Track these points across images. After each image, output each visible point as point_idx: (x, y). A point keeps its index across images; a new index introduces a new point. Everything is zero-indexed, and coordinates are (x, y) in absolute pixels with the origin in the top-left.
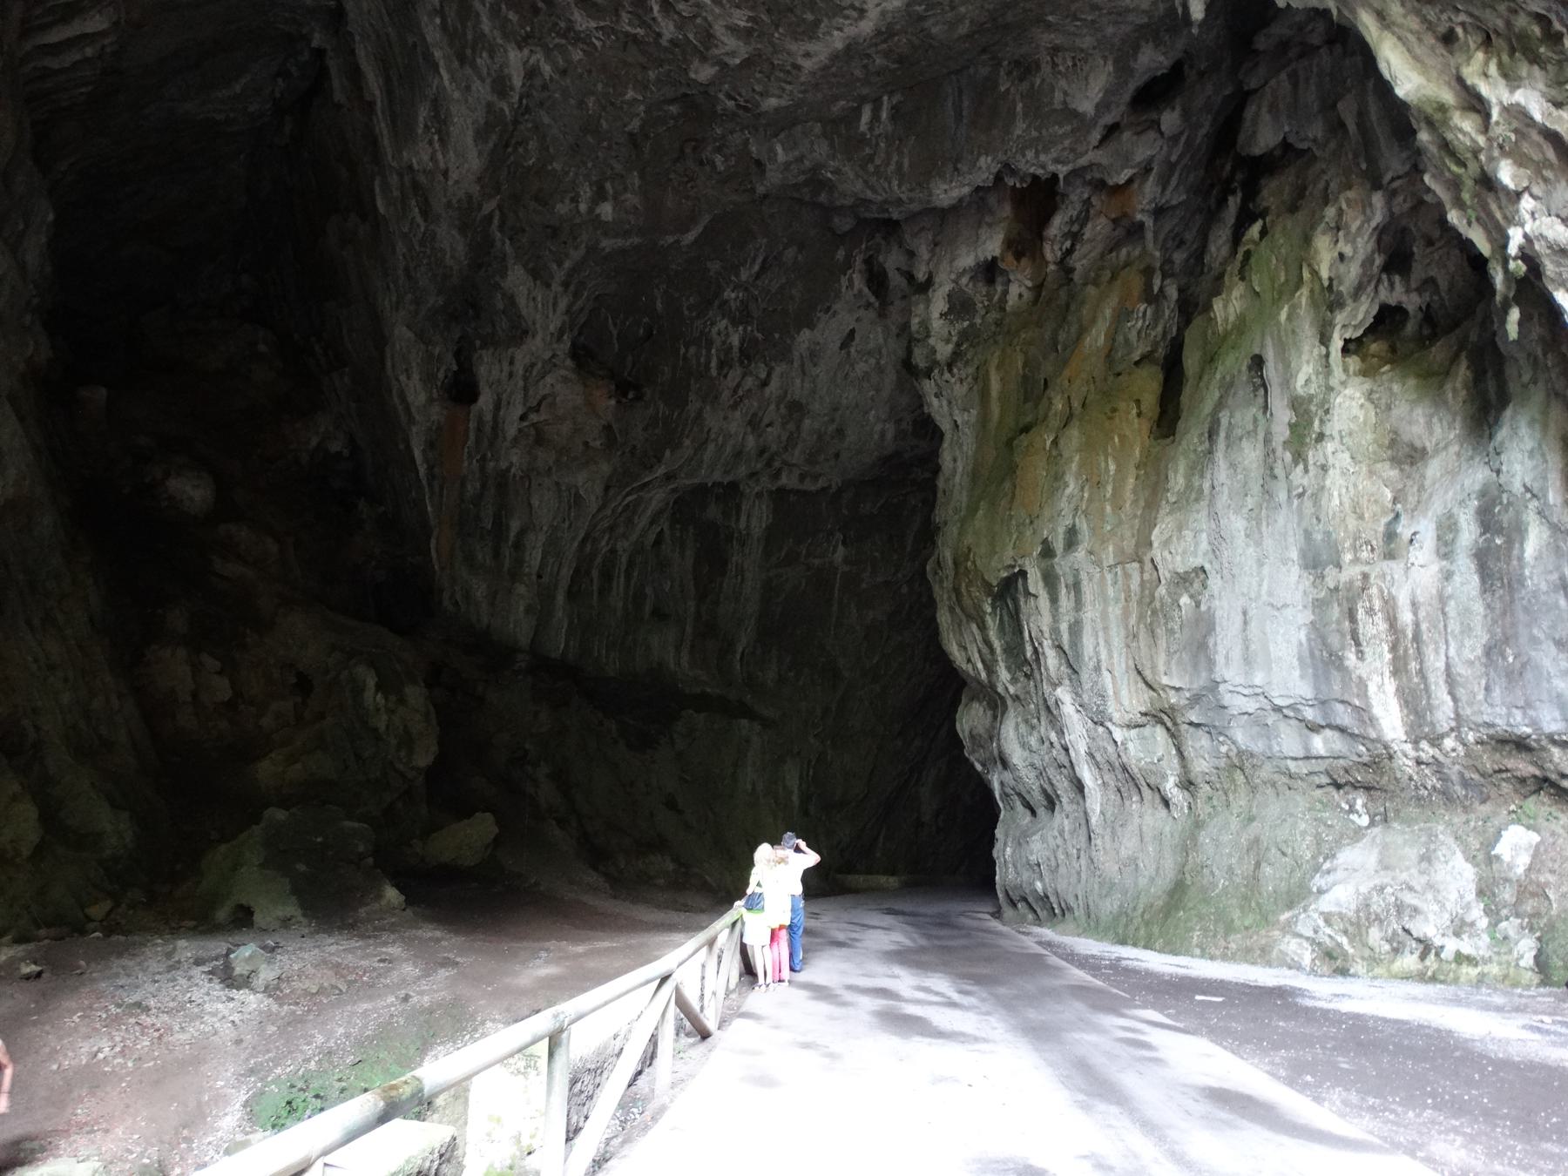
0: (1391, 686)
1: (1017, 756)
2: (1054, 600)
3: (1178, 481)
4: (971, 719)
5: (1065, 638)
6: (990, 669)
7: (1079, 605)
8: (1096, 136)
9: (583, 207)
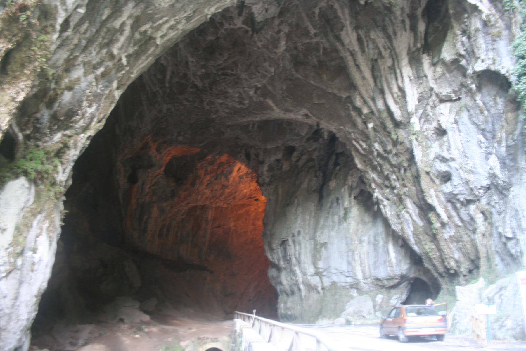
0: (360, 269)
1: (285, 282)
2: (295, 247)
3: (322, 222)
4: (272, 272)
5: (297, 256)
6: (279, 260)
7: (300, 248)
8: (305, 140)
9: (174, 137)
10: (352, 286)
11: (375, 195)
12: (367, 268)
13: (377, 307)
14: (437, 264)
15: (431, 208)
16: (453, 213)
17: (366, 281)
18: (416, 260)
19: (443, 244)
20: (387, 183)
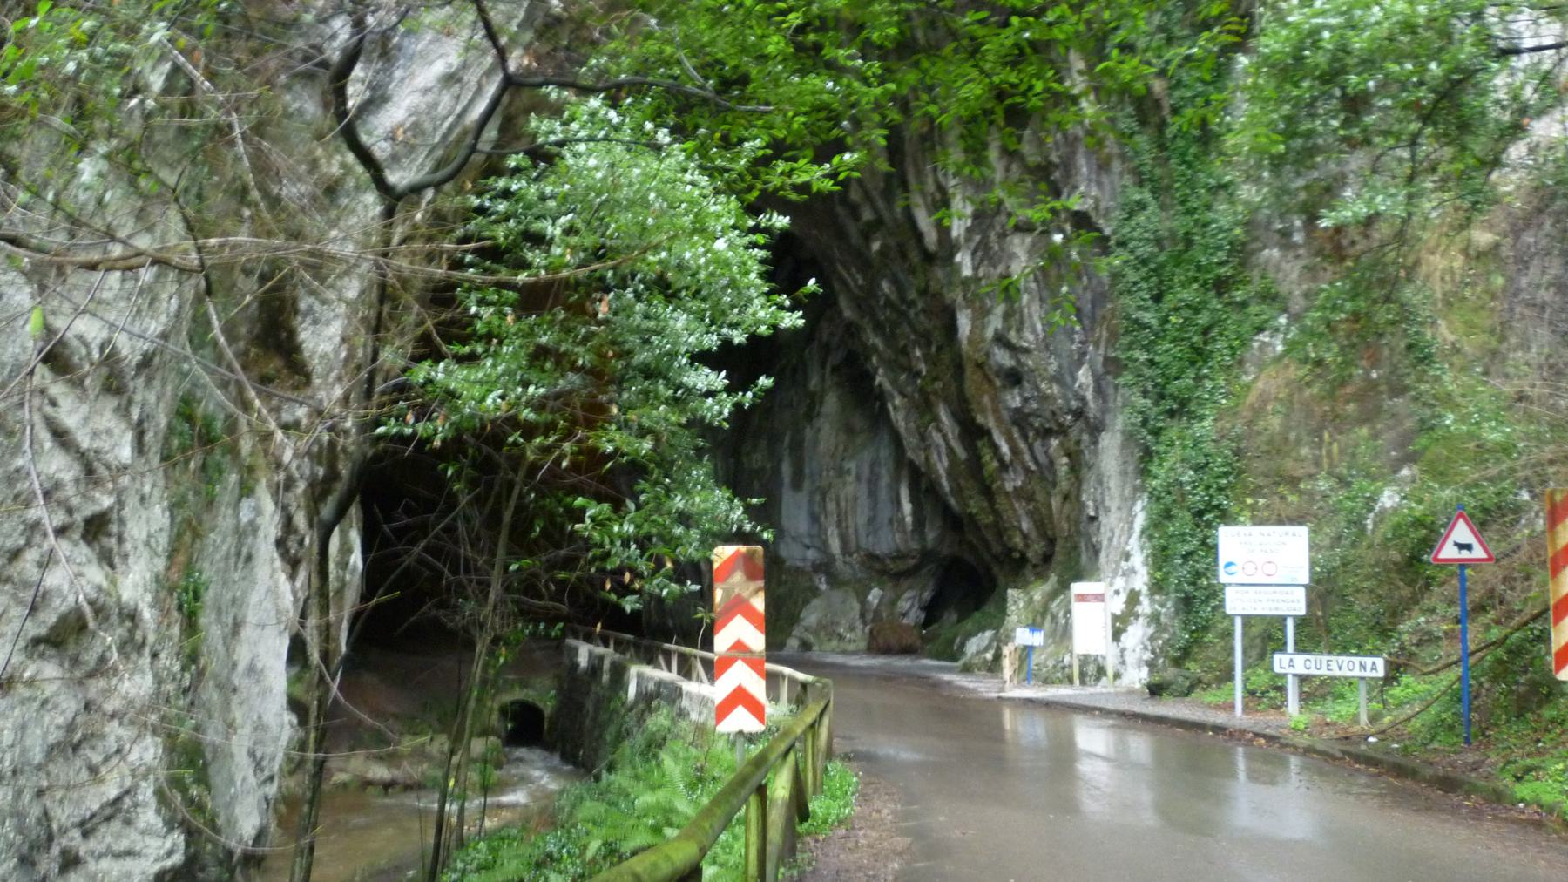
10: (818, 568)
11: (878, 379)
12: (851, 530)
13: (870, 616)
14: (990, 537)
15: (985, 433)
16: (1022, 446)
17: (848, 559)
18: (955, 523)
19: (1001, 503)
20: (903, 360)
